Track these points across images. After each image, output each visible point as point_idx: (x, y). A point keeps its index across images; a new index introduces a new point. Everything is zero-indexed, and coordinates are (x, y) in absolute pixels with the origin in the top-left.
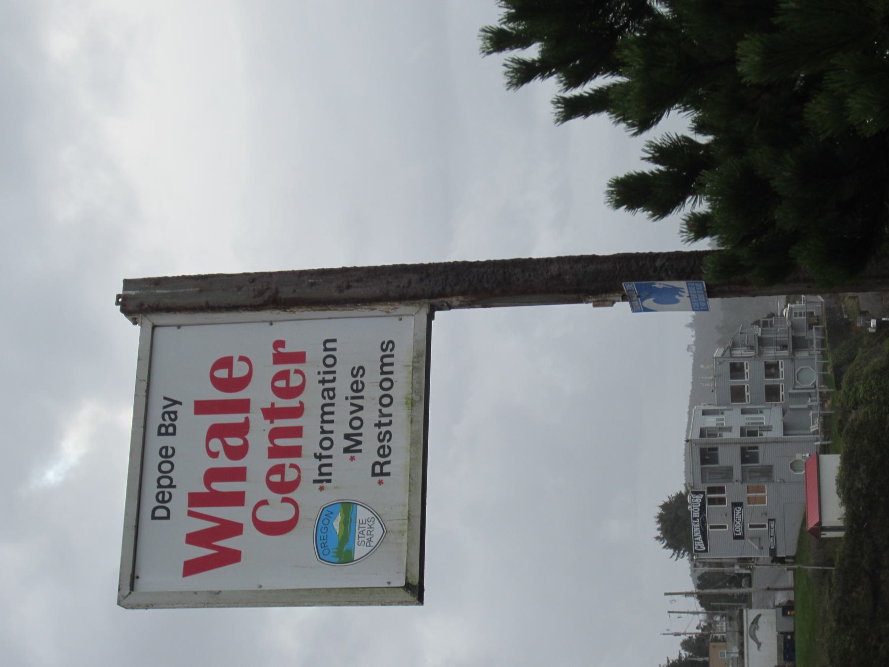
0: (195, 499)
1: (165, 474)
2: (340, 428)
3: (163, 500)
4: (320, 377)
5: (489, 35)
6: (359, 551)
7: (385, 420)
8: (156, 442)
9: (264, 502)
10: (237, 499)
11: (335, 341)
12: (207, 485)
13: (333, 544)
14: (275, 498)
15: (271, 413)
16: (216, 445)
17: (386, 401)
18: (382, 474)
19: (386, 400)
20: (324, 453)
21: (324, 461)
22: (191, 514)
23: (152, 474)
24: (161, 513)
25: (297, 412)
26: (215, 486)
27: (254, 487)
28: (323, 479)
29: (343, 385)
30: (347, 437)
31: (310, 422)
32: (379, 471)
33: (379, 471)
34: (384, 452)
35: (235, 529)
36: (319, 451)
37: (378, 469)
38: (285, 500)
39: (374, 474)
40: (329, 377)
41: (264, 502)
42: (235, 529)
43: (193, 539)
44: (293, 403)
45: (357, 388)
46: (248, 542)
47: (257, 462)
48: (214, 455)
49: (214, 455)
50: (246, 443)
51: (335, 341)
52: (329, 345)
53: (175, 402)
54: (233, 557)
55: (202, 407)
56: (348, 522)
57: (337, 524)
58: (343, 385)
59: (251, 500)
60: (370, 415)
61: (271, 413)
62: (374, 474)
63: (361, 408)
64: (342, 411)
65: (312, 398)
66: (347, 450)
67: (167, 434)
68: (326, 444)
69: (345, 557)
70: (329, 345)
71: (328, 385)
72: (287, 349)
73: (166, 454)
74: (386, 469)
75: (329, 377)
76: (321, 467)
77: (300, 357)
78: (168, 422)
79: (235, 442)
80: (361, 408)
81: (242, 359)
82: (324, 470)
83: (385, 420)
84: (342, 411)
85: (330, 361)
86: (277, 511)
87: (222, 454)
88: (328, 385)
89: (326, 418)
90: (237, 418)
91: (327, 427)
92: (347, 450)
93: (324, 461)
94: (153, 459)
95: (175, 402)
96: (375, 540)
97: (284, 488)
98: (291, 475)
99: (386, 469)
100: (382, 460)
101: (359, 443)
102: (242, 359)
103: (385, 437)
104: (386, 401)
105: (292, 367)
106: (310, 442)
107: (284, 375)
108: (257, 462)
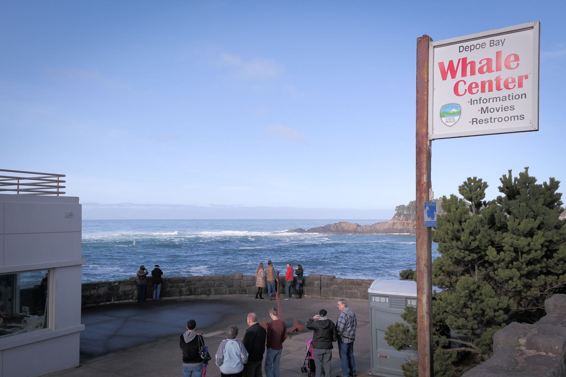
0: (464, 60)
1: (475, 47)
2: (491, 105)
3: (465, 49)
4: (511, 95)
5: (507, 176)
6: (444, 119)
7: (493, 120)
8: (487, 40)
9: (465, 83)
10: (464, 74)
11: (64, 176)
12: (469, 63)
13: (447, 110)
14: (467, 87)
15: (498, 80)
16: (484, 62)
17: (500, 120)
18: (473, 122)
19: (500, 120)
20: (481, 101)
21: (478, 101)
22: (460, 60)
23: (475, 42)
24: (462, 48)
25: (499, 89)
26: (469, 65)
27: (469, 79)
28: (472, 102)
29: (508, 103)
30: (487, 108)
31: (495, 93)
32: (474, 121)
33: (474, 121)
34: (481, 122)
35: (453, 76)
36: (482, 99)
37: (475, 120)
38: (466, 90)
39: (473, 119)
40: (511, 98)
41: (465, 83)
42: (453, 76)
43: (451, 63)
44: (502, 86)
45: (506, 109)
46: (450, 82)
47: (478, 78)
48: (480, 63)
49: (480, 63)
50: (485, 73)
51: (64, 176)
52: (524, 96)
53: (503, 44)
54: (444, 78)
55: (498, 54)
56: (454, 114)
57: (454, 110)
58: (508, 103)
59: (464, 78)
60: (495, 115)
61: (498, 80)
62: (473, 119)
63: (498, 111)
64: (497, 105)
65: (501, 94)
66: (482, 108)
67: (491, 43)
68: (485, 101)
69: (442, 116)
70: (524, 96)
71: (507, 98)
72: (524, 81)
73: (483, 46)
74: (475, 123)
75: (511, 98)
76: (477, 100)
77: (520, 85)
78: (495, 43)
79: (485, 69)
80: (498, 111)
81: (518, 64)
82: (475, 102)
83: (493, 120)
84: (497, 105)
85: (517, 97)
86: (462, 88)
87: (481, 65)
88: (507, 98)
89: (495, 99)
90: (494, 68)
91: (491, 100)
92: (482, 108)
93: (478, 101)
94: (480, 41)
95: (503, 44)
96: (448, 124)
97: (470, 89)
98: (474, 91)
99: (475, 123)
100: (478, 121)
101: (485, 113)
102: (518, 64)
103: (486, 121)
104: (500, 120)
105: (480, 89)
106: (487, 95)
107: (477, 86)
108: (478, 78)
